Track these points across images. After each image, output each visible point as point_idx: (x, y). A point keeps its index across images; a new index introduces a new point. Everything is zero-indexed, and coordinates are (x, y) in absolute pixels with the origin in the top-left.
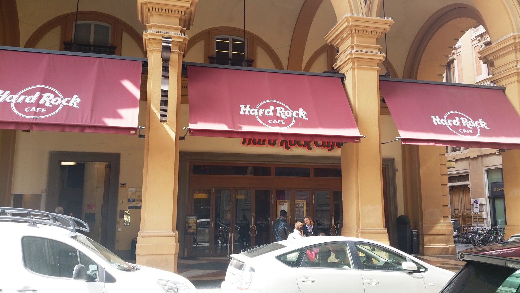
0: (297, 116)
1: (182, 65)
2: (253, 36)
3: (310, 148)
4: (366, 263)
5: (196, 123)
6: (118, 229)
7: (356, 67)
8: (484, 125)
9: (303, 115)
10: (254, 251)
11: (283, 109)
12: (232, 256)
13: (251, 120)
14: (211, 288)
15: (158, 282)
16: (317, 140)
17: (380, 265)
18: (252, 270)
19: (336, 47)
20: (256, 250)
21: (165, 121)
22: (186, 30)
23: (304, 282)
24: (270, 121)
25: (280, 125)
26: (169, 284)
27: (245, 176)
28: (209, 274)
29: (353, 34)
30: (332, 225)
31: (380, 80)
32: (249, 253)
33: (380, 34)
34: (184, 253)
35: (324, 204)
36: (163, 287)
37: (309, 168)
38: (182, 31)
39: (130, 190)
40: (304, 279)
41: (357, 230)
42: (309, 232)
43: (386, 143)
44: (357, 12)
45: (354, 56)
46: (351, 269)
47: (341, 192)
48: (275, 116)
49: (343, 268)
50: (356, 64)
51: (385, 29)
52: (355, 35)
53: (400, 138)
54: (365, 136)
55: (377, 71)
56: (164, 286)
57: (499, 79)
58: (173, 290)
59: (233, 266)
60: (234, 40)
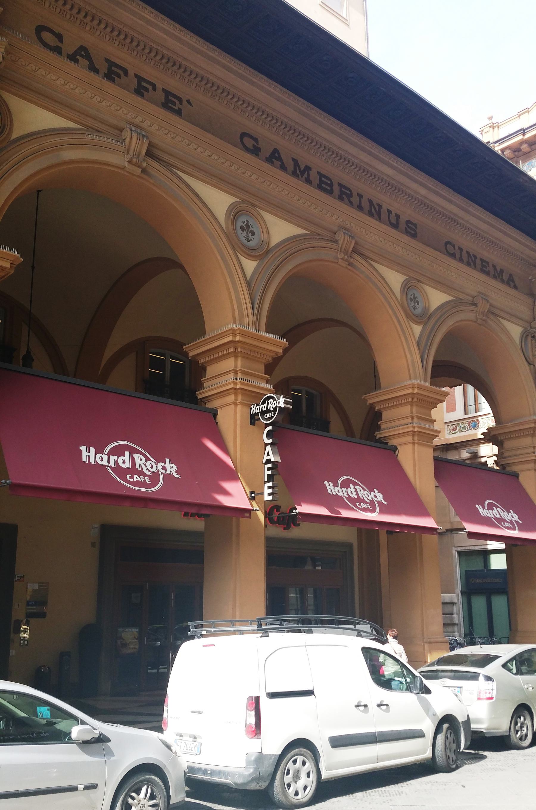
6: (11, 651)
8: (172, 470)
11: (143, 459)
13: (338, 502)
57: (389, 436)
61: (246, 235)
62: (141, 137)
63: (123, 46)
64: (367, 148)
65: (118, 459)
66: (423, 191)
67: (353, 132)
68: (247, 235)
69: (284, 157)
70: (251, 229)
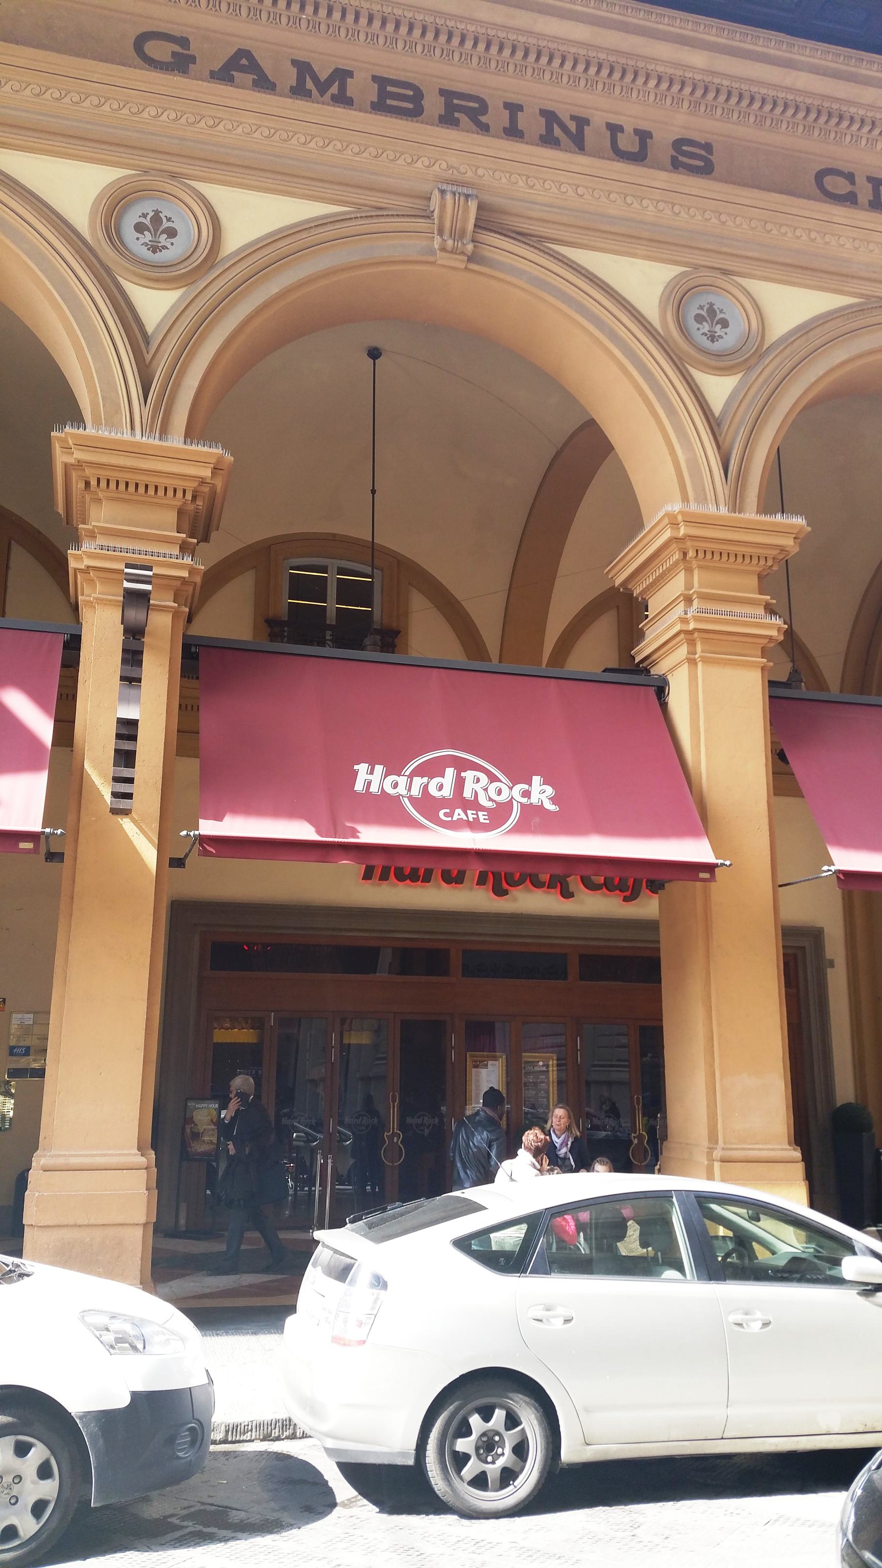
0: (524, 800)
1: (183, 644)
2: (398, 561)
3: (567, 894)
4: (733, 1259)
5: (219, 817)
7: (700, 657)
9: (543, 797)
10: (384, 1221)
12: (318, 1235)
14: (255, 1333)
15: (83, 1317)
16: (587, 871)
17: (777, 1266)
18: (380, 1283)
19: (640, 599)
20: (394, 1217)
21: (126, 812)
22: (198, 542)
23: (541, 1321)
24: (446, 814)
25: (474, 826)
26: (115, 1325)
27: (370, 977)
28: (250, 1286)
29: (690, 562)
30: (635, 1133)
31: (770, 697)
32: (371, 1226)
33: (770, 563)
34: (177, 1216)
35: (614, 1063)
36: (98, 1333)
37: (566, 954)
38: (184, 548)
39: (16, 1019)
40: (540, 1313)
41: (711, 1150)
42: (560, 1158)
43: (796, 883)
44: (702, 499)
45: (692, 626)
46: (685, 1281)
47: (661, 1028)
48: (459, 800)
49: (663, 1276)
50: (699, 648)
51: (782, 549)
52: (694, 564)
53: (833, 868)
54: (728, 863)
55: (763, 669)
56: (101, 1332)
58: (130, 1345)
59: (319, 1268)
60: (341, 571)
61: (708, 329)
62: (462, 198)
63: (779, 123)
64: (661, 27)
65: (428, 783)
66: (698, 59)
67: (634, 6)
68: (712, 330)
69: (266, 65)
70: (166, 224)
